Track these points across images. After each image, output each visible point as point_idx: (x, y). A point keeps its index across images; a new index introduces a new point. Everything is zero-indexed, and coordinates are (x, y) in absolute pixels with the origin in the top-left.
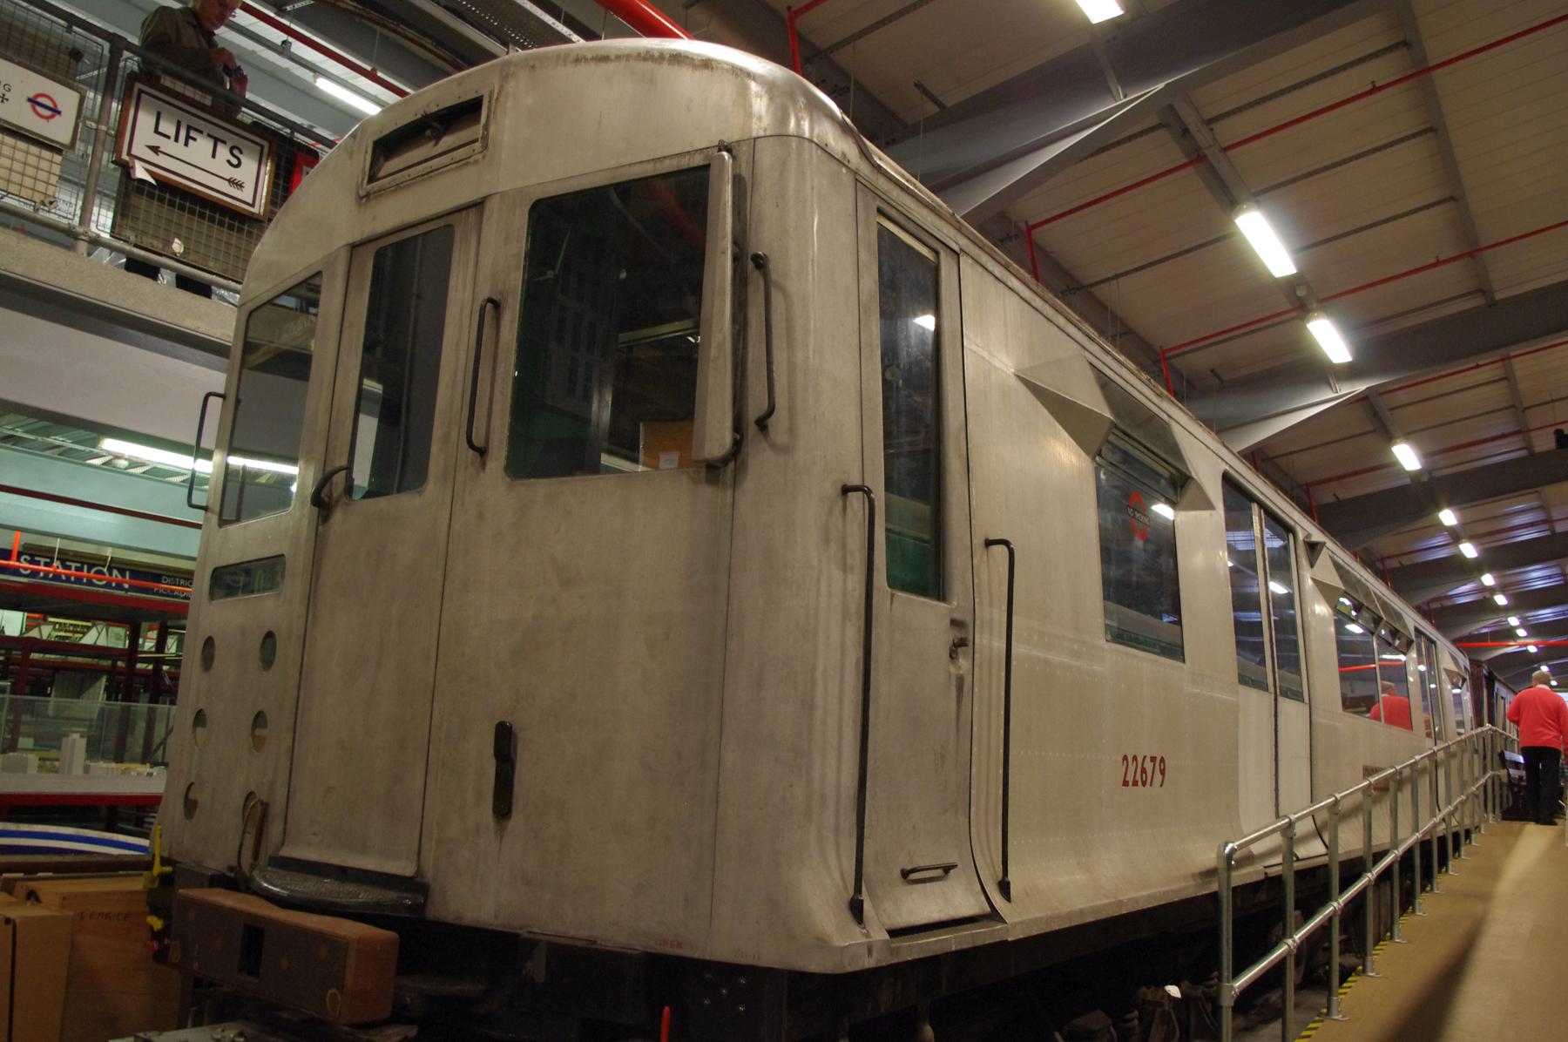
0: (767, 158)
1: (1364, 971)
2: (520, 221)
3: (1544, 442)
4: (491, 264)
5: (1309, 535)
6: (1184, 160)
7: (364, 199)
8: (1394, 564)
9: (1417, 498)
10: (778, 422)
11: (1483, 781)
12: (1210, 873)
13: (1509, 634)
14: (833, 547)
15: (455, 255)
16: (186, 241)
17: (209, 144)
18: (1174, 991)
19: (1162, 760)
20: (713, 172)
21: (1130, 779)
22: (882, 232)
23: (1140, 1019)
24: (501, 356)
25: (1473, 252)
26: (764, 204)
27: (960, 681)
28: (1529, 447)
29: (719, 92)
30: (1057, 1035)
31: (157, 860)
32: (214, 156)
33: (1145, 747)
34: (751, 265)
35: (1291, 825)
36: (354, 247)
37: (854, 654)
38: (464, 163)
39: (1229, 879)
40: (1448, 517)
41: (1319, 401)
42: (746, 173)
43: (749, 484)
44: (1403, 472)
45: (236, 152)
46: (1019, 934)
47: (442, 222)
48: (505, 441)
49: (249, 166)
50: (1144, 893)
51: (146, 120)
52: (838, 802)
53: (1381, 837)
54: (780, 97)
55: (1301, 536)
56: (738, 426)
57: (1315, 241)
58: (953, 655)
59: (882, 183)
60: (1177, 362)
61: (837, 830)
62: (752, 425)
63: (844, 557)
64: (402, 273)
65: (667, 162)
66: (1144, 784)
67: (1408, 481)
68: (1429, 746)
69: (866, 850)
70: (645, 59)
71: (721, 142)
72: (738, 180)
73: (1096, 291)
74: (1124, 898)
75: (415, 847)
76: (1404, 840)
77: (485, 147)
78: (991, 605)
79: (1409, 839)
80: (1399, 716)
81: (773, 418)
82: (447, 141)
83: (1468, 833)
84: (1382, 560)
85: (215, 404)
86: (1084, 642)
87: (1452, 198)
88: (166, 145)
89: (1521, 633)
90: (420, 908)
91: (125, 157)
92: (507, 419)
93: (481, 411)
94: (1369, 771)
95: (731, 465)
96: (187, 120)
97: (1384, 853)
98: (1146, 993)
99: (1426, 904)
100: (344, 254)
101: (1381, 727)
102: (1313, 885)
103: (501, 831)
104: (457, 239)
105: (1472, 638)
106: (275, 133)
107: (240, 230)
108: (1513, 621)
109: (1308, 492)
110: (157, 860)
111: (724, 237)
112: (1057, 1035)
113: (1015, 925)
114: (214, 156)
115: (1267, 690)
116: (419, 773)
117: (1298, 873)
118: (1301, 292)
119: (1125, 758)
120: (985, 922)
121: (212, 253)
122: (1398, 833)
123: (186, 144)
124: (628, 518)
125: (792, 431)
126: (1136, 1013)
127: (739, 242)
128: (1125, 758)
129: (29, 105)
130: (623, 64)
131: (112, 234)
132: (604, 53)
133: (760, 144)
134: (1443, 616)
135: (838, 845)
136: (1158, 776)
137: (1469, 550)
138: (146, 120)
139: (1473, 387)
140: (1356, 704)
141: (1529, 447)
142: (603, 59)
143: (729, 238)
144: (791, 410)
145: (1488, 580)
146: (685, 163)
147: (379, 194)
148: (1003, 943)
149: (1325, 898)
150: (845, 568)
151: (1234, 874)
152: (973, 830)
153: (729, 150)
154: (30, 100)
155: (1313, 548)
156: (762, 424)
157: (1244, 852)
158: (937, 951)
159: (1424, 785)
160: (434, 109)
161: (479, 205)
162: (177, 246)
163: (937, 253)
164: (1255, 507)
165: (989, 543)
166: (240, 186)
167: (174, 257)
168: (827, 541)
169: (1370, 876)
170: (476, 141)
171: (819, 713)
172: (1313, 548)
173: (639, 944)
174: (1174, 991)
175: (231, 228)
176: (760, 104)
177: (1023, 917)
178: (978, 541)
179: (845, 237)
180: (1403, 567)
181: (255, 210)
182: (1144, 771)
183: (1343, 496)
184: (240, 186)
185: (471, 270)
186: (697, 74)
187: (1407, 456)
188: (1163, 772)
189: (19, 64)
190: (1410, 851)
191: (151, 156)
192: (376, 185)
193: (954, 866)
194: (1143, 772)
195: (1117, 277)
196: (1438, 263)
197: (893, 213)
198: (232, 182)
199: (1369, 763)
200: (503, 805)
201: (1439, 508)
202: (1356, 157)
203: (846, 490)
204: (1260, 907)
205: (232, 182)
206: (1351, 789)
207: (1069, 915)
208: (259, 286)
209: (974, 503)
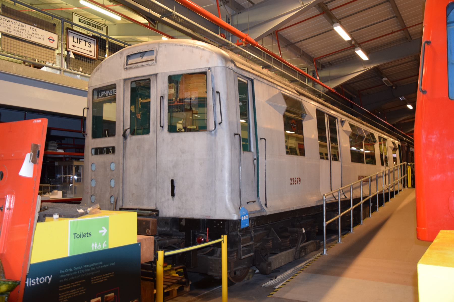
21: (292, 183)
33: (296, 176)
36: (125, 80)
41: (359, 71)
51: (71, 39)
55: (339, 119)
56: (215, 125)
73: (296, 44)
83: (397, 192)
88: (76, 44)
94: (360, 178)
96: (80, 37)
97: (368, 197)
100: (122, 82)
102: (346, 204)
103: (173, 200)
122: (371, 191)
124: (195, 141)
131: (67, 68)
162: (81, 69)
165: (261, 139)
167: (80, 72)
172: (342, 122)
175: (90, 63)
177: (269, 211)
181: (95, 57)
182: (295, 181)
188: (300, 181)
189: (46, 30)
192: (128, 66)
196: (393, 32)
198: (90, 51)
199: (360, 175)
200: (173, 194)
202: (266, 173)
203: (235, 134)
205: (90, 51)
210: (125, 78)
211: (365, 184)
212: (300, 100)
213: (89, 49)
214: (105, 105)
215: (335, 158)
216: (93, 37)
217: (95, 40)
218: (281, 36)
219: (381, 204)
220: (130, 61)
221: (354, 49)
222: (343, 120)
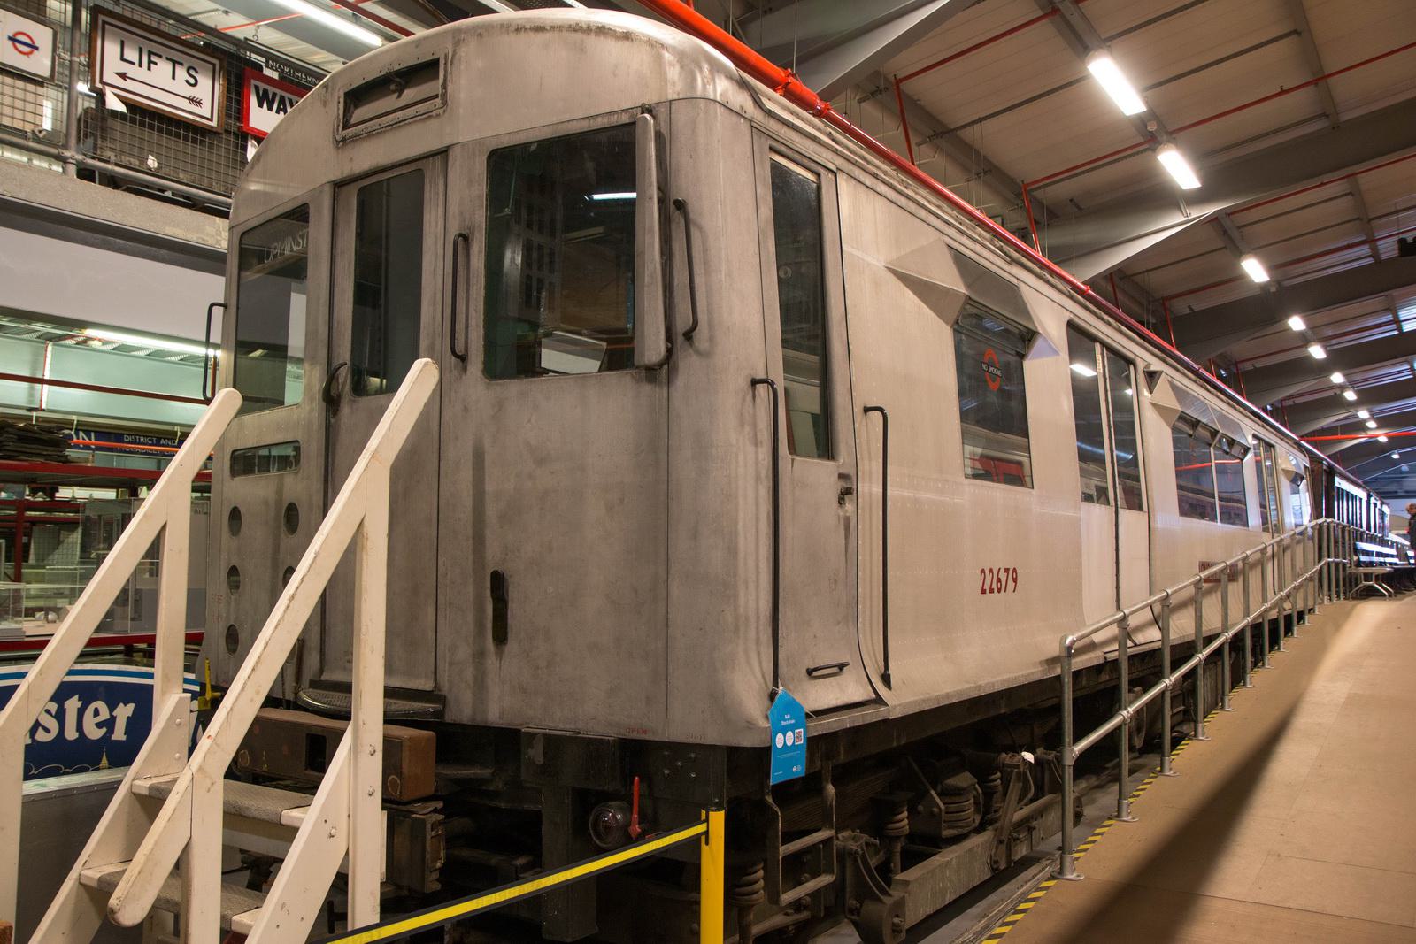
0: (681, 116)
1: (1195, 735)
2: (480, 167)
3: (1388, 248)
4: (457, 206)
5: (1149, 365)
6: (1040, 13)
7: (341, 143)
8: (1248, 366)
9: (1268, 306)
10: (701, 334)
11: (1318, 567)
12: (1053, 661)
13: (1360, 426)
14: (747, 429)
15: (427, 195)
16: (158, 156)
17: (169, 66)
18: (1029, 756)
19: (1015, 570)
20: (639, 130)
21: (987, 587)
22: (776, 167)
23: (1001, 779)
24: (473, 280)
25: (1319, 79)
26: (681, 157)
27: (847, 521)
28: (1375, 254)
29: (635, 61)
30: (933, 792)
31: (208, 687)
32: (174, 77)
33: (999, 562)
34: (672, 207)
35: (1125, 618)
36: (338, 185)
37: (765, 509)
38: (428, 116)
39: (1069, 664)
40: (1296, 323)
42: (664, 130)
43: (680, 381)
44: (1251, 284)
45: (192, 72)
46: (896, 714)
47: (413, 167)
48: (482, 349)
49: (205, 82)
50: (999, 679)
51: (111, 49)
52: (758, 622)
53: (1212, 621)
54: (688, 62)
55: (1141, 366)
56: (669, 338)
57: (1162, 81)
58: (841, 502)
59: (773, 125)
60: (1039, 194)
61: (758, 642)
62: (682, 337)
63: (756, 435)
64: (382, 212)
65: (599, 119)
66: (999, 591)
67: (1258, 292)
68: (1268, 540)
69: (780, 656)
70: (575, 30)
71: (643, 104)
72: (659, 136)
73: (961, 133)
74: (982, 683)
75: (433, 668)
76: (1235, 624)
77: (445, 103)
78: (870, 460)
79: (1240, 623)
80: (1235, 514)
81: (697, 330)
82: (410, 94)
83: (1301, 616)
84: (1236, 363)
85: (218, 312)
86: (947, 481)
87: (1295, 32)
88: (132, 71)
89: (1372, 424)
90: (439, 714)
91: (99, 85)
92: (482, 332)
93: (460, 327)
95: (665, 367)
96: (148, 46)
97: (1217, 636)
98: (1005, 757)
99: (1257, 679)
100: (328, 191)
101: (1219, 525)
102: (1147, 666)
104: (427, 181)
105: (1323, 431)
106: (224, 52)
107: (202, 142)
108: (1363, 414)
109: (1163, 304)
110: (208, 687)
111: (651, 185)
112: (933, 792)
113: (895, 707)
114: (174, 77)
115: (1108, 504)
116: (431, 610)
117: (1131, 657)
118: (1152, 127)
119: (983, 571)
120: (872, 706)
121: (181, 165)
122: (1229, 616)
123: (149, 69)
125: (711, 339)
126: (999, 774)
127: (663, 188)
128: (983, 571)
129: (10, 43)
130: (557, 33)
132: (538, 24)
133: (674, 105)
134: (1289, 414)
135: (759, 653)
136: (1010, 581)
137: (1317, 352)
138: (111, 49)
139: (1318, 204)
140: (1194, 505)
141: (1375, 254)
142: (539, 29)
143: (655, 184)
144: (711, 326)
145: (1337, 378)
146: (615, 120)
147: (355, 139)
148: (886, 721)
149: (1159, 676)
150: (756, 443)
151: (1073, 661)
152: (861, 636)
153: (650, 112)
154: (10, 38)
155: (1152, 377)
156: (688, 336)
157: (1086, 641)
158: (836, 728)
159: (1254, 578)
160: (397, 68)
161: (444, 153)
162: (152, 162)
163: (818, 175)
164: (1098, 347)
165: (867, 410)
166: (199, 103)
168: (742, 425)
169: (1202, 656)
170: (436, 97)
171: (741, 555)
172: (1152, 377)
173: (612, 734)
174: (1029, 756)
175: (195, 141)
176: (674, 73)
177: (901, 700)
178: (858, 410)
179: (745, 176)
180: (1256, 370)
181: (214, 124)
182: (999, 580)
183: (1196, 308)
184: (199, 103)
185: (441, 209)
186: (620, 44)
187: (1255, 270)
188: (1015, 580)
190: (1241, 633)
191: (119, 82)
192: (350, 132)
193: (847, 664)
194: (998, 582)
195: (980, 120)
196: (1283, 92)
197: (783, 149)
198: (191, 100)
201: (1288, 316)
203: (754, 382)
204: (1097, 690)
205: (191, 100)
206: (1181, 585)
207: (937, 698)
208: (248, 215)
209: (853, 378)
210: (336, 175)
211: (1209, 592)
212: (1015, 281)
213: (189, 91)
214: (378, 921)
215: (1134, 499)
216: (209, 49)
217: (216, 62)
218: (916, 105)
219: (1258, 659)
220: (360, 113)
221: (1154, 150)
222: (1153, 368)
